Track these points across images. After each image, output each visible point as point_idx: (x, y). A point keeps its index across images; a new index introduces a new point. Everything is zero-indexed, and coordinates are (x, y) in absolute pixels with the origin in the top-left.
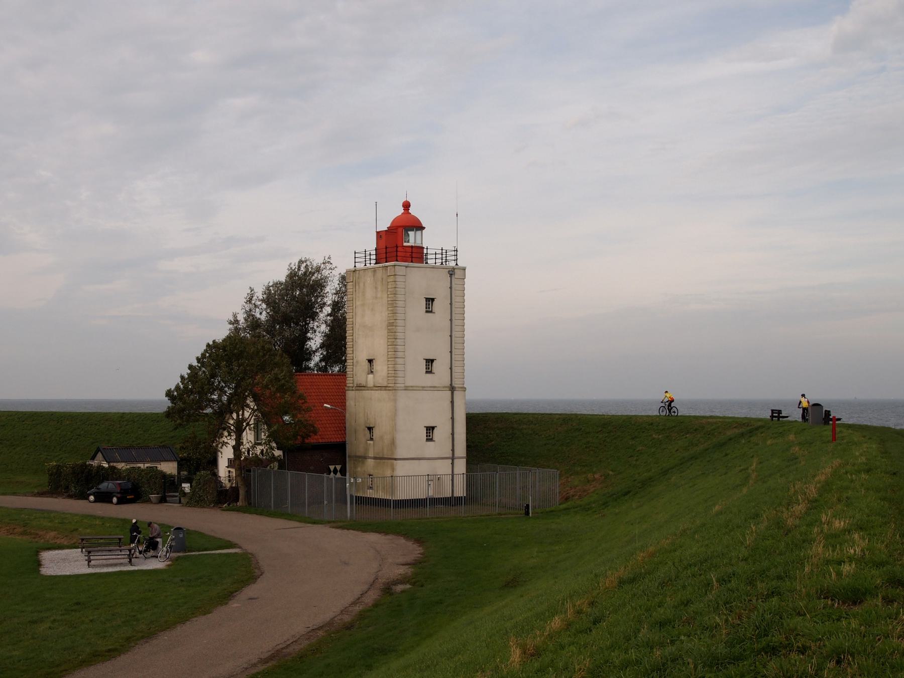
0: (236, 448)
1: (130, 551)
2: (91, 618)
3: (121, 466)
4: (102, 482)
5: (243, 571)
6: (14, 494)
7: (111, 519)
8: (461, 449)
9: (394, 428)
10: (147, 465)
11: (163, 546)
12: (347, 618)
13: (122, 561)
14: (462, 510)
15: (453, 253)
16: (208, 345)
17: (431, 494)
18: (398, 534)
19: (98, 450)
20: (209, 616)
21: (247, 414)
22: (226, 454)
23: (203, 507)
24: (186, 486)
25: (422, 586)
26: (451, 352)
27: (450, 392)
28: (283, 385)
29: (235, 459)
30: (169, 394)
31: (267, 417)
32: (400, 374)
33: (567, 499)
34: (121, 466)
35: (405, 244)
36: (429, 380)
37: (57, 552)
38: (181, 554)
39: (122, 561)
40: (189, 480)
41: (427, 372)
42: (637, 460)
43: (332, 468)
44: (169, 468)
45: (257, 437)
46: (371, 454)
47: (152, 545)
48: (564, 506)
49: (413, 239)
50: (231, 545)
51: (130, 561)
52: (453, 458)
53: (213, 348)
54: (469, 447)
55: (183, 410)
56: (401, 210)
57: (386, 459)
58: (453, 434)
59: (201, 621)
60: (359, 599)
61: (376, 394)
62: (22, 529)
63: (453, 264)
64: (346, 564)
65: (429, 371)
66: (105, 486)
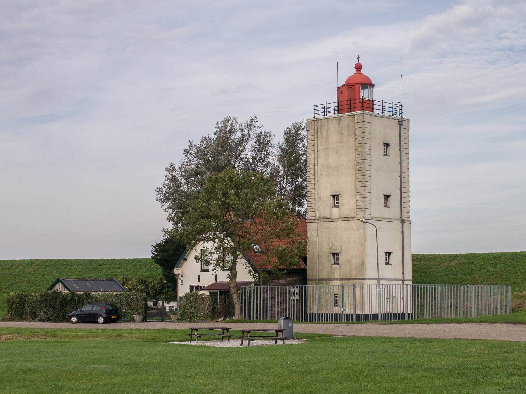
8: (409, 275)
26: (401, 190)
46: (337, 276)
49: (365, 94)
57: (354, 280)
58: (403, 259)
66: (87, 309)
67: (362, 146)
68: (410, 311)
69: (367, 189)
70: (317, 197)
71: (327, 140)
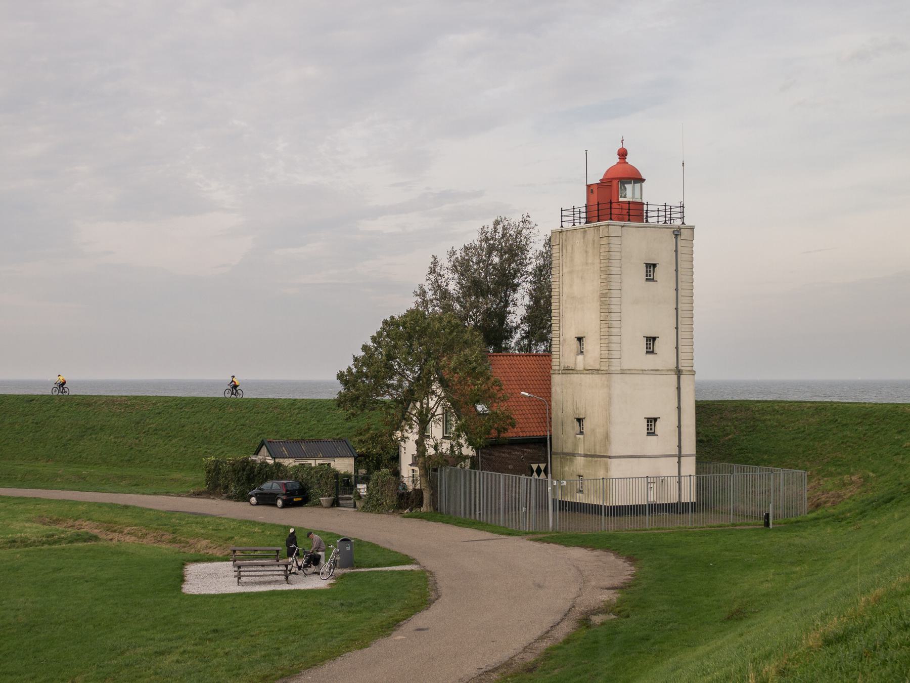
0: (420, 443)
1: (286, 566)
2: (227, 650)
3: (289, 462)
4: (266, 480)
5: (413, 593)
6: (167, 494)
7: (274, 526)
8: (690, 445)
9: (608, 419)
10: (319, 462)
11: (326, 561)
12: (530, 658)
13: (278, 578)
14: (688, 521)
15: (679, 210)
16: (385, 322)
17: (653, 499)
18: (608, 549)
19: (263, 444)
20: (366, 650)
21: (432, 404)
22: (408, 450)
23: (381, 513)
24: (362, 488)
25: (628, 616)
26: (677, 328)
27: (676, 376)
28: (474, 369)
29: (418, 456)
30: (341, 376)
31: (459, 405)
32: (615, 355)
33: (818, 506)
34: (289, 462)
35: (621, 199)
36: (650, 362)
37: (205, 564)
38: (347, 571)
39: (278, 578)
40: (365, 480)
41: (647, 352)
42: (903, 459)
43: (535, 466)
44: (344, 465)
45: (446, 429)
47: (314, 560)
48: (813, 515)
49: (630, 193)
50: (408, 560)
51: (287, 578)
52: (680, 456)
53: (391, 324)
54: (700, 442)
55: (357, 398)
56: (616, 160)
58: (679, 427)
59: (356, 656)
60: (547, 632)
61: (588, 379)
62: (171, 537)
63: (678, 222)
64: (539, 586)
65: (650, 351)
66: (270, 486)
67: (606, 271)
68: (694, 499)
69: (614, 331)
70: (561, 339)
71: (572, 260)
